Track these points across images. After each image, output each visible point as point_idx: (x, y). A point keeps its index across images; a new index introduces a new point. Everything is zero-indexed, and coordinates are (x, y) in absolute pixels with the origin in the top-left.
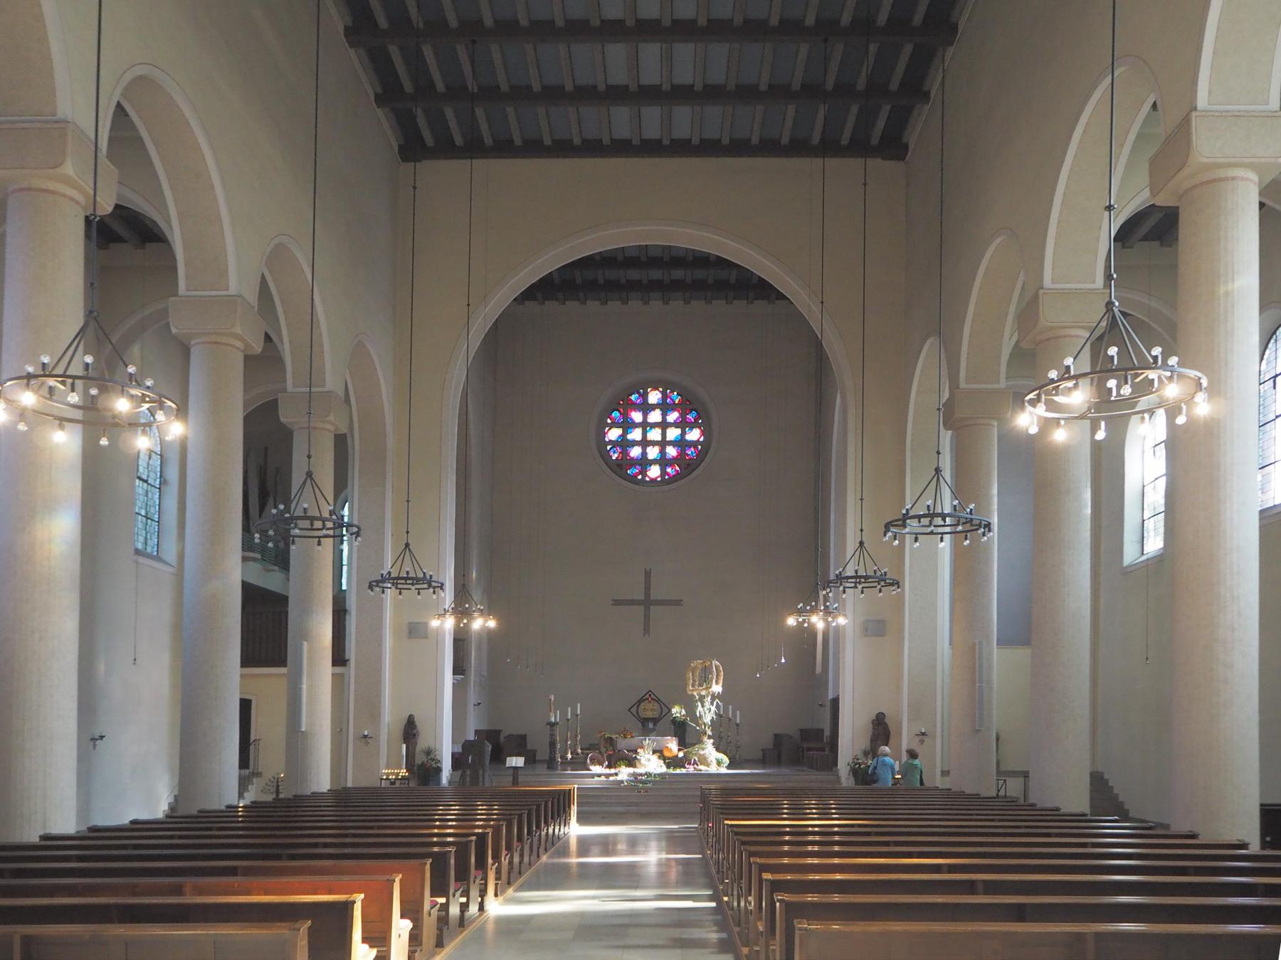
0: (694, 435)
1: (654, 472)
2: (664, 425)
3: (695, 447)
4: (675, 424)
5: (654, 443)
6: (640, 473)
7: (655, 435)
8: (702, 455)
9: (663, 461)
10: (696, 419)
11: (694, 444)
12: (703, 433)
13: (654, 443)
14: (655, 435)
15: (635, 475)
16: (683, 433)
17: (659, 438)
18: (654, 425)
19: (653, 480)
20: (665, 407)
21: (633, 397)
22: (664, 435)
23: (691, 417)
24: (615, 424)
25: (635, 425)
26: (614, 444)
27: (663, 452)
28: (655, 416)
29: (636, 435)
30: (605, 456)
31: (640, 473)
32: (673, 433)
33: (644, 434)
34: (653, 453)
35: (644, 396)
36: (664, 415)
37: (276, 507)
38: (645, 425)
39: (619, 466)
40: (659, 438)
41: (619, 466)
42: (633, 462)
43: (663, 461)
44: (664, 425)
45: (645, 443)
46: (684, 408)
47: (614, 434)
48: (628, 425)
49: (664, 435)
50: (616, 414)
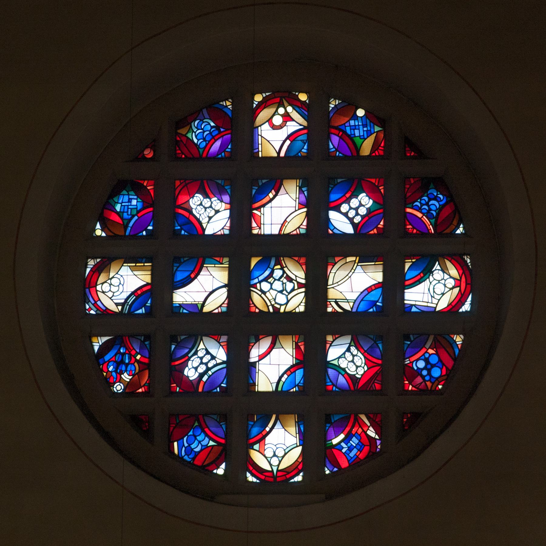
0: (434, 291)
1: (280, 446)
2: (316, 249)
3: (442, 344)
4: (361, 246)
5: (276, 325)
6: (222, 454)
7: (280, 291)
8: (466, 374)
9: (313, 400)
10: (444, 223)
11: (434, 325)
12: (468, 283)
13: (276, 325)
14: (280, 291)
15: (203, 465)
16: (393, 285)
17: (297, 303)
18: (278, 248)
19: (275, 481)
20: (320, 172)
21: (198, 133)
22: (316, 288)
23: (424, 210)
24: (122, 249)
25: (207, 249)
26: (120, 325)
27: (311, 360)
28: (281, 212)
29: (206, 289)
30: (80, 378)
31: (222, 454)
32: (352, 283)
33: (239, 287)
34: (274, 366)
35: (240, 127)
36: (316, 208)
37: (120, 380)
38: (244, 251)
39: (140, 423)
40: (297, 303)
41: (223, 392)
42: (387, 368)
43: (313, 400)
44: (316, 249)
45: (242, 324)
46: (396, 175)
47: (121, 285)
48: (176, 250)
49: (316, 288)
50: (128, 203)
